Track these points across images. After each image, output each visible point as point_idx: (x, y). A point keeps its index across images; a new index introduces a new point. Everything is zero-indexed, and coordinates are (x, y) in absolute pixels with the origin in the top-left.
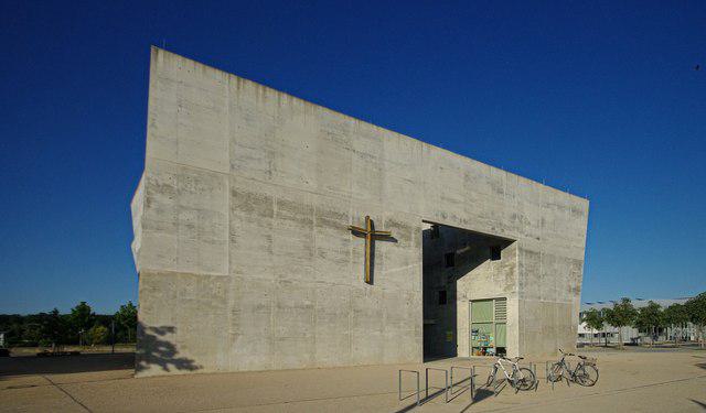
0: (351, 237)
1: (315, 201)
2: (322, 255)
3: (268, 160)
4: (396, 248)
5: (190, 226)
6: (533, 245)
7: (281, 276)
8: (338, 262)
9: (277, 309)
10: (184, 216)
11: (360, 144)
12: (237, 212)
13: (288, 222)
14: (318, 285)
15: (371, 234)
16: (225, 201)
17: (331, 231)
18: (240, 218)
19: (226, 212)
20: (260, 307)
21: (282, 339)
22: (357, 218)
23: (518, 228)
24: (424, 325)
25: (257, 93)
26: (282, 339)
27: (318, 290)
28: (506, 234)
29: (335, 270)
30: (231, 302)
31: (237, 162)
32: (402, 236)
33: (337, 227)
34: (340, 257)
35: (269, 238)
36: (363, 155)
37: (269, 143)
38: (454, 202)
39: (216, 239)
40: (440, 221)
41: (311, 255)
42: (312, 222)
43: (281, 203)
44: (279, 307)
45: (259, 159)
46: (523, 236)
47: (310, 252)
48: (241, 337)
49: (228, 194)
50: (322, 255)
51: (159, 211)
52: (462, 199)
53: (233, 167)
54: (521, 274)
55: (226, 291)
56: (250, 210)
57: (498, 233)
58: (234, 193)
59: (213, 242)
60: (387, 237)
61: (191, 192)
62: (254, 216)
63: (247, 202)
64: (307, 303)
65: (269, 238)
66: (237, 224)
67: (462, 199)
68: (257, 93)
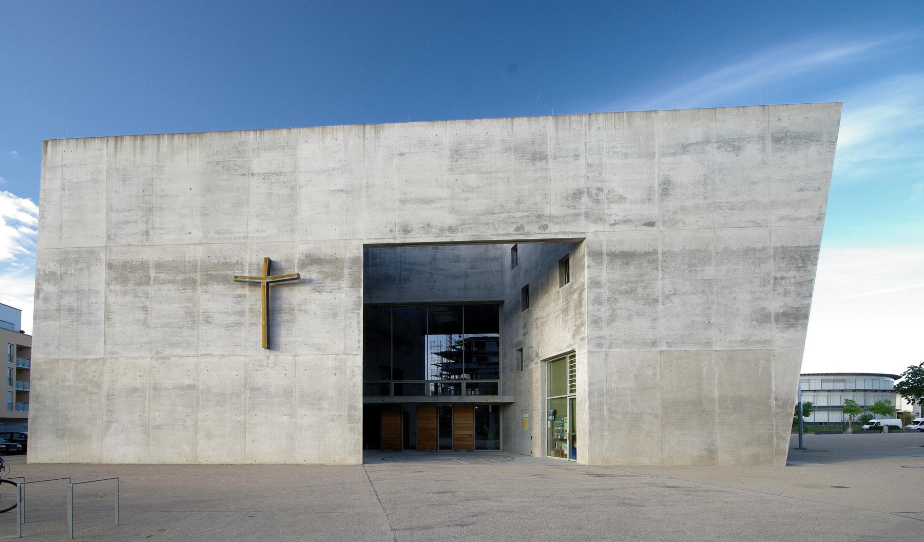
0: (645, 228)
1: (197, 254)
2: (208, 321)
3: (144, 219)
4: (316, 296)
5: (70, 310)
6: (633, 238)
7: (158, 352)
8: (228, 327)
9: (152, 392)
10: (68, 300)
11: (260, 163)
12: (111, 287)
13: (166, 287)
14: (203, 359)
15: (274, 280)
16: (100, 274)
17: (217, 287)
18: (115, 291)
19: (101, 287)
20: (135, 390)
21: (159, 427)
22: (252, 262)
23: (587, 215)
24: (366, 407)
25: (135, 147)
26: (159, 427)
27: (203, 366)
28: (581, 236)
29: (225, 340)
30: (105, 388)
31: (114, 230)
32: (327, 276)
33: (224, 280)
34: (231, 319)
35: (145, 309)
36: (266, 176)
37: (147, 198)
38: (427, 201)
39: (92, 319)
40: (31, 394)
41: (194, 322)
42: (194, 281)
43: (159, 266)
44: (155, 389)
45: (136, 222)
46: (608, 228)
47: (193, 318)
48: (115, 424)
49: (103, 269)
50: (208, 321)
51: (46, 300)
52: (444, 193)
53: (109, 238)
54: (597, 301)
55: (101, 374)
56: (124, 280)
57: (555, 232)
58: (110, 266)
59: (90, 323)
60: (295, 281)
61: (71, 275)
62: (130, 287)
63: (128, 273)
64: (188, 382)
65: (145, 309)
66: (112, 299)
67: (444, 193)
68: (135, 147)
